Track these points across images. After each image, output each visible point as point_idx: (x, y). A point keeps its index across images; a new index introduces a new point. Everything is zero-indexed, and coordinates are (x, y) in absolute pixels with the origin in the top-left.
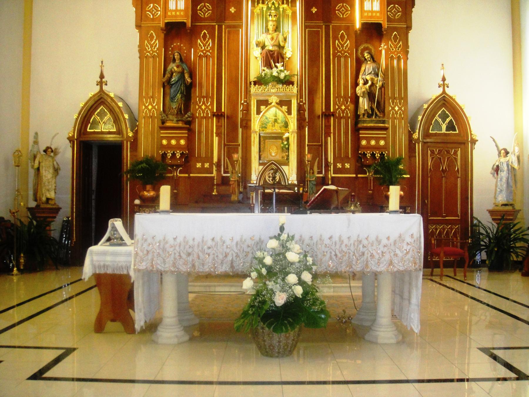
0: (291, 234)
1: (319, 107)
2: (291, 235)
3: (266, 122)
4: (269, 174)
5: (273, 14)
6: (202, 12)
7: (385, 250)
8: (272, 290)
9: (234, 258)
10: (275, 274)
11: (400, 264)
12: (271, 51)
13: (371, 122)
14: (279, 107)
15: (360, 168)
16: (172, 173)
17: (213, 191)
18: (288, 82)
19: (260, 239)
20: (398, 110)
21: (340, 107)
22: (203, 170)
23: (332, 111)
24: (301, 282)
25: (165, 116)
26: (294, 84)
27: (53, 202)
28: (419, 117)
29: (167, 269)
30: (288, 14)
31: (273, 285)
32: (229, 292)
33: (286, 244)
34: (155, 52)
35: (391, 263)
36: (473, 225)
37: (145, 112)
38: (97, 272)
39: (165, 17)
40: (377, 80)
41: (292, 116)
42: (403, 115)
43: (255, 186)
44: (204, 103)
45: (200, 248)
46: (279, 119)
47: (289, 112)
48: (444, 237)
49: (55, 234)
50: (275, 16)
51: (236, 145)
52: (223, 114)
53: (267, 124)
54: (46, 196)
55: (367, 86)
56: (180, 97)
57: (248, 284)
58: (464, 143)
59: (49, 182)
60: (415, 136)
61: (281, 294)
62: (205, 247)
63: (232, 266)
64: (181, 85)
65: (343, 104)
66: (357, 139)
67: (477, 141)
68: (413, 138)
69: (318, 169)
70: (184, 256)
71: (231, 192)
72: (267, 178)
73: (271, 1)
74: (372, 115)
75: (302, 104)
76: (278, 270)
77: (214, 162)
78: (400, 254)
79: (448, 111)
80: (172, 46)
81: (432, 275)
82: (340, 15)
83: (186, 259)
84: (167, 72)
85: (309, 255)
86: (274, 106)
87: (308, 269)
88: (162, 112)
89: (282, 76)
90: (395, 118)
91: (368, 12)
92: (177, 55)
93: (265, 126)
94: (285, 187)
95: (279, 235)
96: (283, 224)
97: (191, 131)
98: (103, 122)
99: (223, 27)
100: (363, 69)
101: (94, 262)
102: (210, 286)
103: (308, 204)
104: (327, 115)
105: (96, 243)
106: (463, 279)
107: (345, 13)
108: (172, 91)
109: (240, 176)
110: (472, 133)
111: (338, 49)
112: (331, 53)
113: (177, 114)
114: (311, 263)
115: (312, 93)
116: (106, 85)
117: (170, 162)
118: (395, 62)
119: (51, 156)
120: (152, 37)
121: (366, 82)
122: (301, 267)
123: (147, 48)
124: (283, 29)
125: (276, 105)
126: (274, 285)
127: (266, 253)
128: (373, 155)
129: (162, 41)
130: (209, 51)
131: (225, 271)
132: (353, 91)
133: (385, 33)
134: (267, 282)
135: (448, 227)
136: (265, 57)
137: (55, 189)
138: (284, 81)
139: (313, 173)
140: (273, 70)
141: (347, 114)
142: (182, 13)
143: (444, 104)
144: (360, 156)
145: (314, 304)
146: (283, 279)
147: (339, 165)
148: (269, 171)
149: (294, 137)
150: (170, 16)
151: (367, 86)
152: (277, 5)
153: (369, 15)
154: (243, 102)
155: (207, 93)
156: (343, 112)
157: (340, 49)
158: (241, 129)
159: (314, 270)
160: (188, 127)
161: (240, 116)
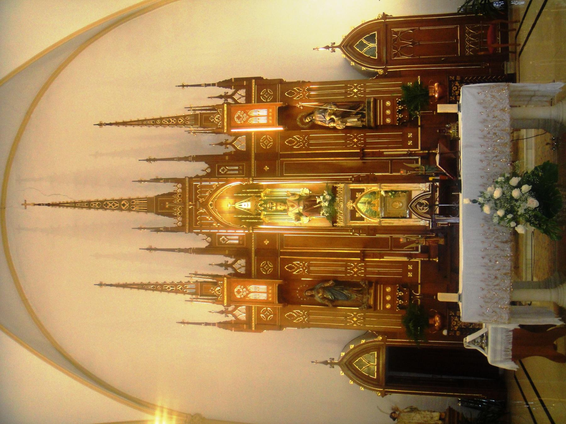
0: (479, 194)
1: (354, 162)
2: (480, 193)
3: (370, 212)
4: (420, 209)
5: (271, 205)
6: (268, 269)
7: (491, 115)
8: (525, 210)
9: (500, 240)
10: (512, 207)
11: (504, 102)
12: (304, 207)
13: (369, 114)
14: (357, 200)
15: (410, 123)
16: (418, 300)
17: (435, 261)
18: (334, 192)
19: (483, 219)
20: (357, 89)
21: (355, 143)
22: (415, 271)
23: (359, 151)
24: (519, 186)
25: (364, 305)
26: (336, 186)
27: (444, 414)
28: (363, 69)
29: (508, 296)
30: (269, 192)
31: (522, 209)
32: (532, 246)
33: (487, 198)
34: (304, 313)
35: (503, 110)
36: (465, 12)
37: (359, 324)
38: (511, 357)
39: (274, 303)
40: (330, 110)
41: (365, 188)
42: (362, 85)
43: (432, 221)
44: (352, 269)
45: (491, 268)
46: (368, 200)
47: (361, 191)
48: (477, 40)
49: (475, 414)
50: (272, 204)
51: (391, 241)
52: (362, 252)
53: (372, 211)
54: (437, 420)
55: (336, 119)
56: (346, 291)
57: (520, 229)
58: (387, 25)
59: (424, 417)
60: (381, 72)
61: (528, 202)
62: (490, 264)
63: (506, 242)
64: (336, 290)
65: (352, 140)
66: (386, 127)
67: (384, 13)
68: (383, 74)
69: (413, 163)
70: (497, 282)
71: (436, 244)
72: (424, 211)
73: (259, 208)
74: (362, 114)
75: (353, 179)
76: (508, 205)
77: (408, 260)
78: (495, 102)
79: (357, 42)
80: (299, 297)
81: (515, 52)
82: (271, 144)
83: (500, 280)
84: (323, 302)
85: (497, 180)
86: (356, 205)
87: (508, 179)
88: (360, 307)
89: (328, 197)
90: (365, 92)
91: (268, 119)
92: (308, 293)
93: (375, 213)
94: (433, 194)
95: (480, 204)
96: (471, 201)
97: (378, 282)
98: (368, 363)
99: (281, 250)
100: (320, 123)
101: (502, 359)
102: (526, 265)
103: (452, 178)
104: (363, 155)
105: (486, 358)
106: (519, 24)
107: (269, 141)
108: (340, 298)
109: (421, 236)
110: (377, 18)
111: (301, 146)
112: (305, 152)
113: (362, 294)
114: (503, 178)
115: (342, 169)
116: (333, 359)
117: (406, 301)
118: (312, 93)
119: (399, 414)
120: (290, 316)
121: (332, 120)
122: (506, 186)
123: (300, 320)
124: (282, 196)
125: (355, 203)
126: (521, 208)
127: (495, 215)
128: (400, 112)
129: (294, 306)
130: (304, 264)
131: (510, 247)
132: (340, 132)
133: (287, 104)
134: (519, 213)
135: (467, 37)
136: (310, 213)
137: (431, 412)
138: (333, 196)
139: (418, 168)
140: (323, 205)
141: (361, 137)
142: (270, 288)
143: (350, 46)
144: (401, 123)
145: (537, 175)
146: (517, 200)
147: (410, 143)
148: (417, 209)
149: (385, 186)
150: (273, 299)
151: (336, 119)
152: (262, 202)
153: (271, 119)
154: (351, 233)
155: (342, 266)
156: (360, 140)
157: (301, 144)
158: (377, 235)
159: (509, 176)
160: (375, 284)
161: (364, 236)
